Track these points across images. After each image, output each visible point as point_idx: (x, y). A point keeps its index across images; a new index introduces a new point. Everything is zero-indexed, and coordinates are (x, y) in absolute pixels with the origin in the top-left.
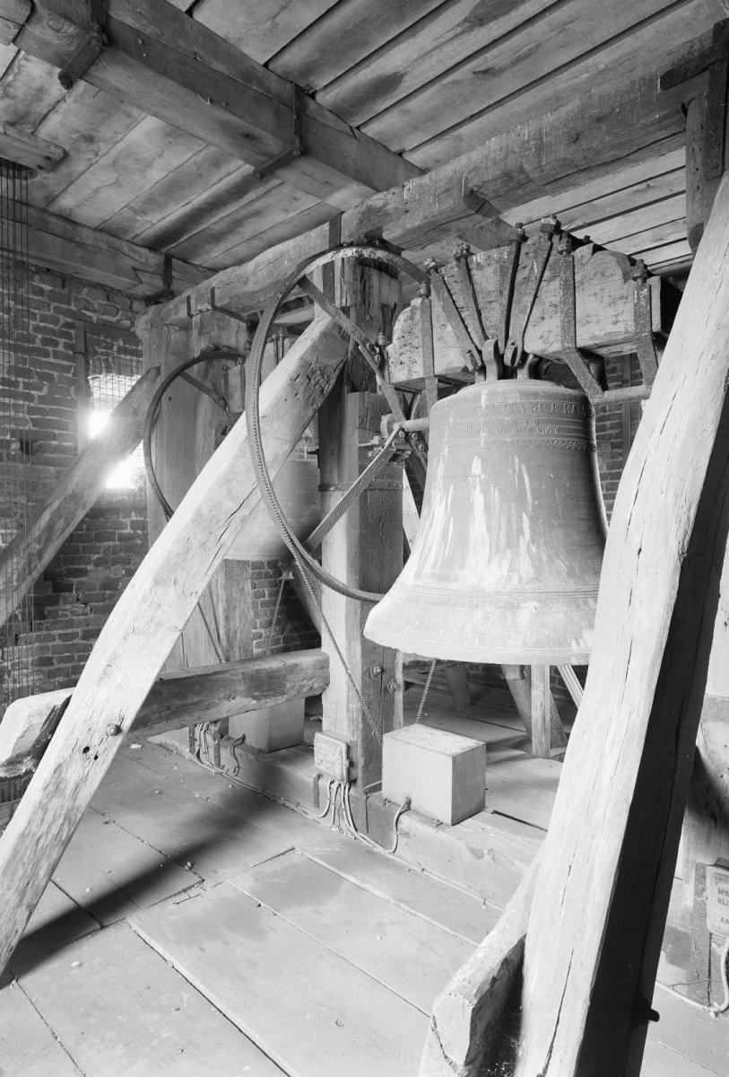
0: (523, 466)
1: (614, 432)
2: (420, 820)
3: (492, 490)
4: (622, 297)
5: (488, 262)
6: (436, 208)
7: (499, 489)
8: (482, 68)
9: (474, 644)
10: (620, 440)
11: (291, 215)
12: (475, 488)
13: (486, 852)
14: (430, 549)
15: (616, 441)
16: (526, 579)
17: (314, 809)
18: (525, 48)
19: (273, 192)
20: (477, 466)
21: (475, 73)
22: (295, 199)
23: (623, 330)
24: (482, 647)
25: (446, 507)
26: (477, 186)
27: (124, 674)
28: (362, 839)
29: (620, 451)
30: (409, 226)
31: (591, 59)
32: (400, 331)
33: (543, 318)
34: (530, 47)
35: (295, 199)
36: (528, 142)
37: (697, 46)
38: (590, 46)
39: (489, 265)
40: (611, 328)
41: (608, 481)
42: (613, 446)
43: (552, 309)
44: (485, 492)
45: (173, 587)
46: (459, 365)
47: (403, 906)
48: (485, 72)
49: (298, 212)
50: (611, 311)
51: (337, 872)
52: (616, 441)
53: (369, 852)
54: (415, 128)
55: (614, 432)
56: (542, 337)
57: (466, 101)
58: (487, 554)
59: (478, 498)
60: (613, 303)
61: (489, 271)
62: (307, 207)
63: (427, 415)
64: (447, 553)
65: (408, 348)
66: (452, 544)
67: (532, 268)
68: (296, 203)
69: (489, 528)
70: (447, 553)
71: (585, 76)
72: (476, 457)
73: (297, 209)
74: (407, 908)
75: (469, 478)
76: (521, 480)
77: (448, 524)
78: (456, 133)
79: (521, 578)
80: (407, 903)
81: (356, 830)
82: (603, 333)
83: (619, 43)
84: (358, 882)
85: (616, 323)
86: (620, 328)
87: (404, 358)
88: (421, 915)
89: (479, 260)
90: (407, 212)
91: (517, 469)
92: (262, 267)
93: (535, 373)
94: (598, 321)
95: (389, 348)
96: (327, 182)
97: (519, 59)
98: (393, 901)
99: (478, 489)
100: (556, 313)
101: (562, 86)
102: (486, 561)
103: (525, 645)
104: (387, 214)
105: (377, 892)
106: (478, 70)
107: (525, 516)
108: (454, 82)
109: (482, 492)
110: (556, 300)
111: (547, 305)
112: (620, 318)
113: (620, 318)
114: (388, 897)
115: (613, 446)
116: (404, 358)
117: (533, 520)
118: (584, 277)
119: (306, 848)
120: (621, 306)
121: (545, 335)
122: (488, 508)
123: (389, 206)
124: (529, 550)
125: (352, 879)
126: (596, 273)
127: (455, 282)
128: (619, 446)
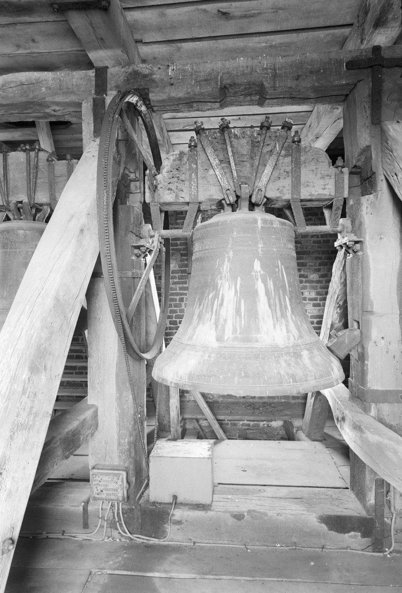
0: (283, 267)
1: (182, 247)
2: (190, 509)
3: (268, 281)
4: (328, 176)
5: (243, 136)
6: (197, 90)
7: (273, 281)
8: (224, 11)
9: (290, 383)
10: (185, 252)
11: (20, 51)
12: (257, 279)
13: (245, 514)
14: (225, 321)
15: (184, 252)
16: (296, 338)
17: (83, 531)
18: (253, 11)
19: (18, 27)
20: (257, 265)
21: (219, 11)
22: (33, 41)
23: (328, 193)
24: (295, 384)
25: (236, 292)
26: (230, 84)
27: (13, 478)
28: (136, 539)
29: (185, 258)
30: (173, 95)
31: (274, 36)
32: (169, 167)
33: (279, 178)
34: (256, 11)
35: (33, 41)
36: (266, 69)
37: (364, 54)
38: (279, 29)
39: (243, 137)
40: (321, 191)
41: (179, 274)
42: (182, 255)
43: (285, 173)
44: (265, 282)
45: (44, 372)
46: (217, 198)
47: (208, 577)
48: (224, 14)
49: (29, 51)
50: (322, 182)
51: (140, 574)
52: (184, 252)
53: (148, 547)
54: (159, 29)
55: (182, 247)
56: (278, 189)
57: (200, 27)
58: (272, 322)
59: (260, 286)
60: (323, 177)
61: (244, 141)
62: (38, 51)
63: (307, 225)
64: (243, 322)
65: (176, 179)
66: (246, 317)
67: (275, 147)
68: (32, 44)
69: (270, 306)
70: (243, 322)
71: (264, 44)
72: (256, 259)
73: (29, 48)
74: (211, 577)
75: (253, 273)
76: (283, 275)
77: (240, 304)
78: (179, 45)
79: (294, 337)
80: (209, 573)
81: (131, 534)
82: (316, 193)
83: (289, 35)
84: (163, 575)
85: (324, 189)
86: (326, 192)
87: (173, 186)
88: (224, 577)
89: (236, 133)
90: (172, 84)
91: (280, 268)
92: (12, 85)
93: (269, 210)
94: (314, 186)
95: (159, 177)
96: (102, 39)
97: (245, 16)
98: (198, 576)
99: (260, 280)
100: (288, 176)
101: (250, 44)
102: (272, 326)
103: (316, 378)
104: (153, 81)
105: (182, 576)
106: (222, 10)
107: (287, 298)
108: (205, 11)
109: (262, 282)
110: (289, 169)
111: (282, 171)
112: (327, 187)
113: (327, 187)
114: (193, 576)
115: (182, 255)
116: (173, 186)
117: (290, 300)
118: (306, 159)
119: (101, 566)
120: (327, 180)
121: (281, 188)
122: (267, 293)
123: (154, 76)
124: (292, 318)
125: (157, 574)
126: (313, 159)
127: (217, 142)
128: (186, 255)
